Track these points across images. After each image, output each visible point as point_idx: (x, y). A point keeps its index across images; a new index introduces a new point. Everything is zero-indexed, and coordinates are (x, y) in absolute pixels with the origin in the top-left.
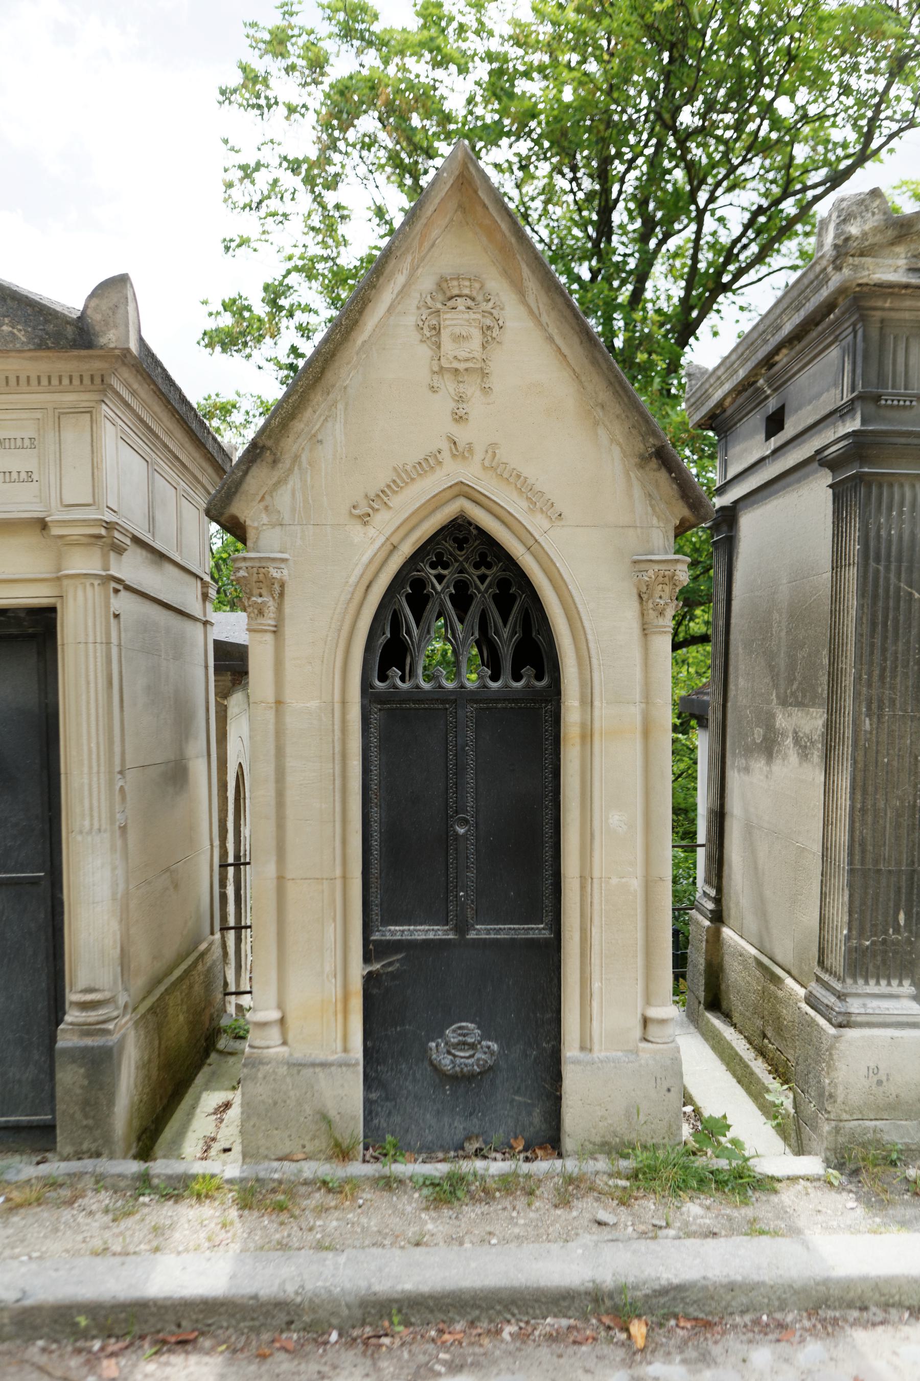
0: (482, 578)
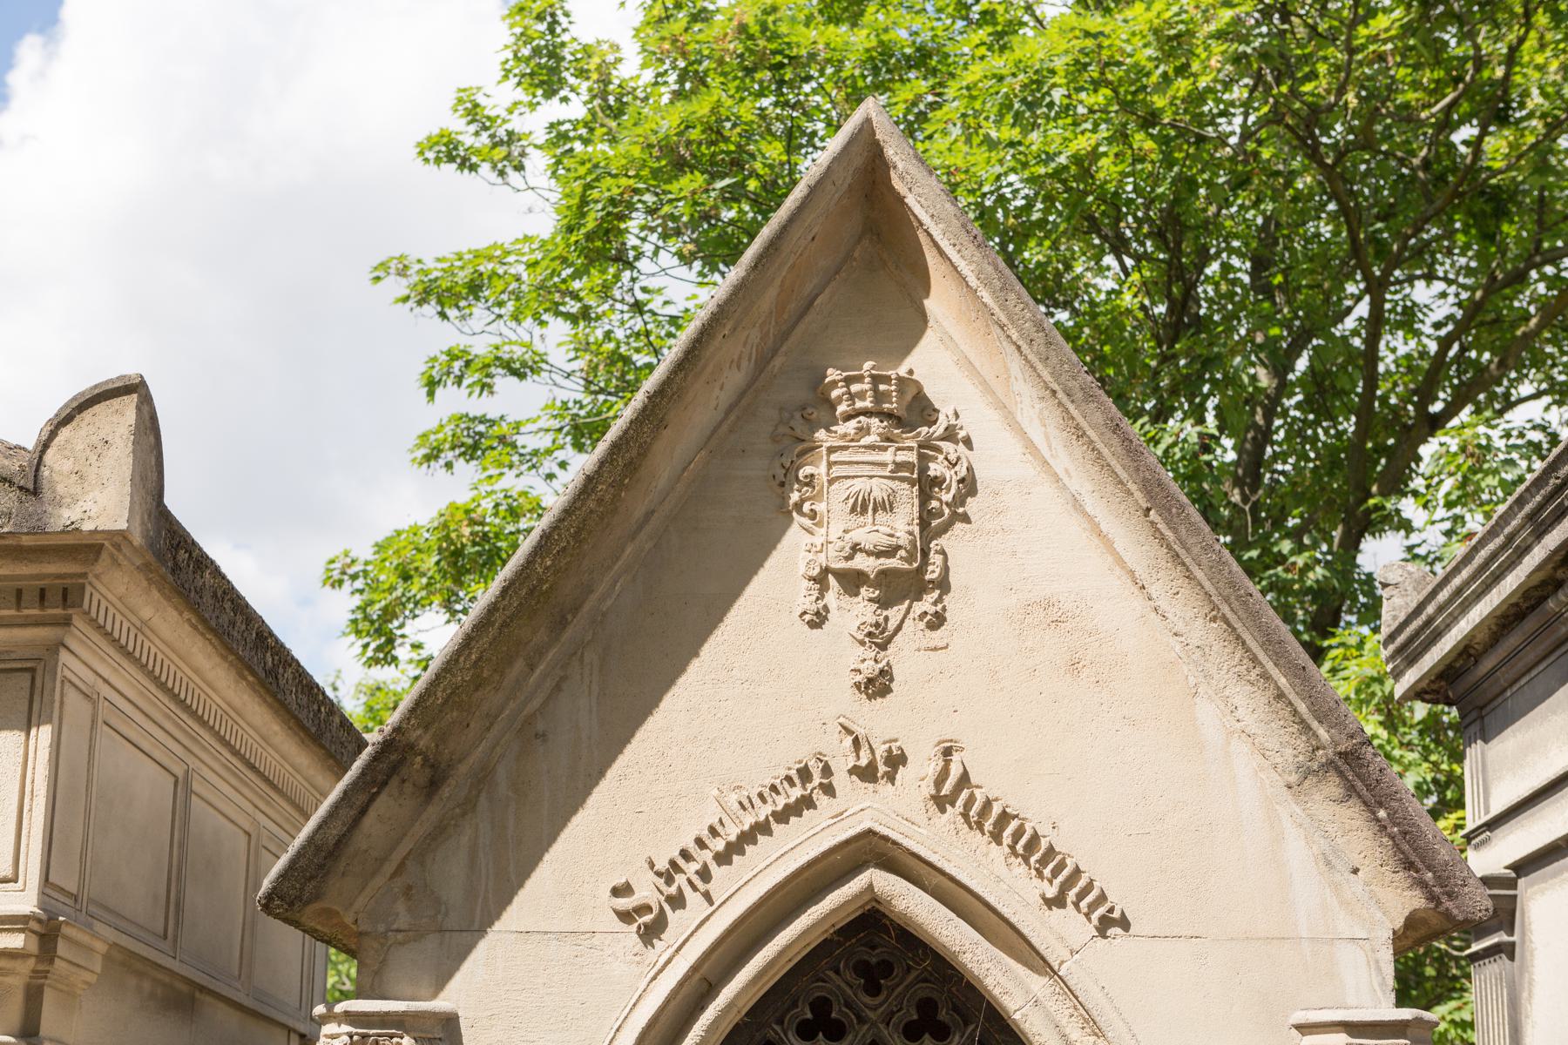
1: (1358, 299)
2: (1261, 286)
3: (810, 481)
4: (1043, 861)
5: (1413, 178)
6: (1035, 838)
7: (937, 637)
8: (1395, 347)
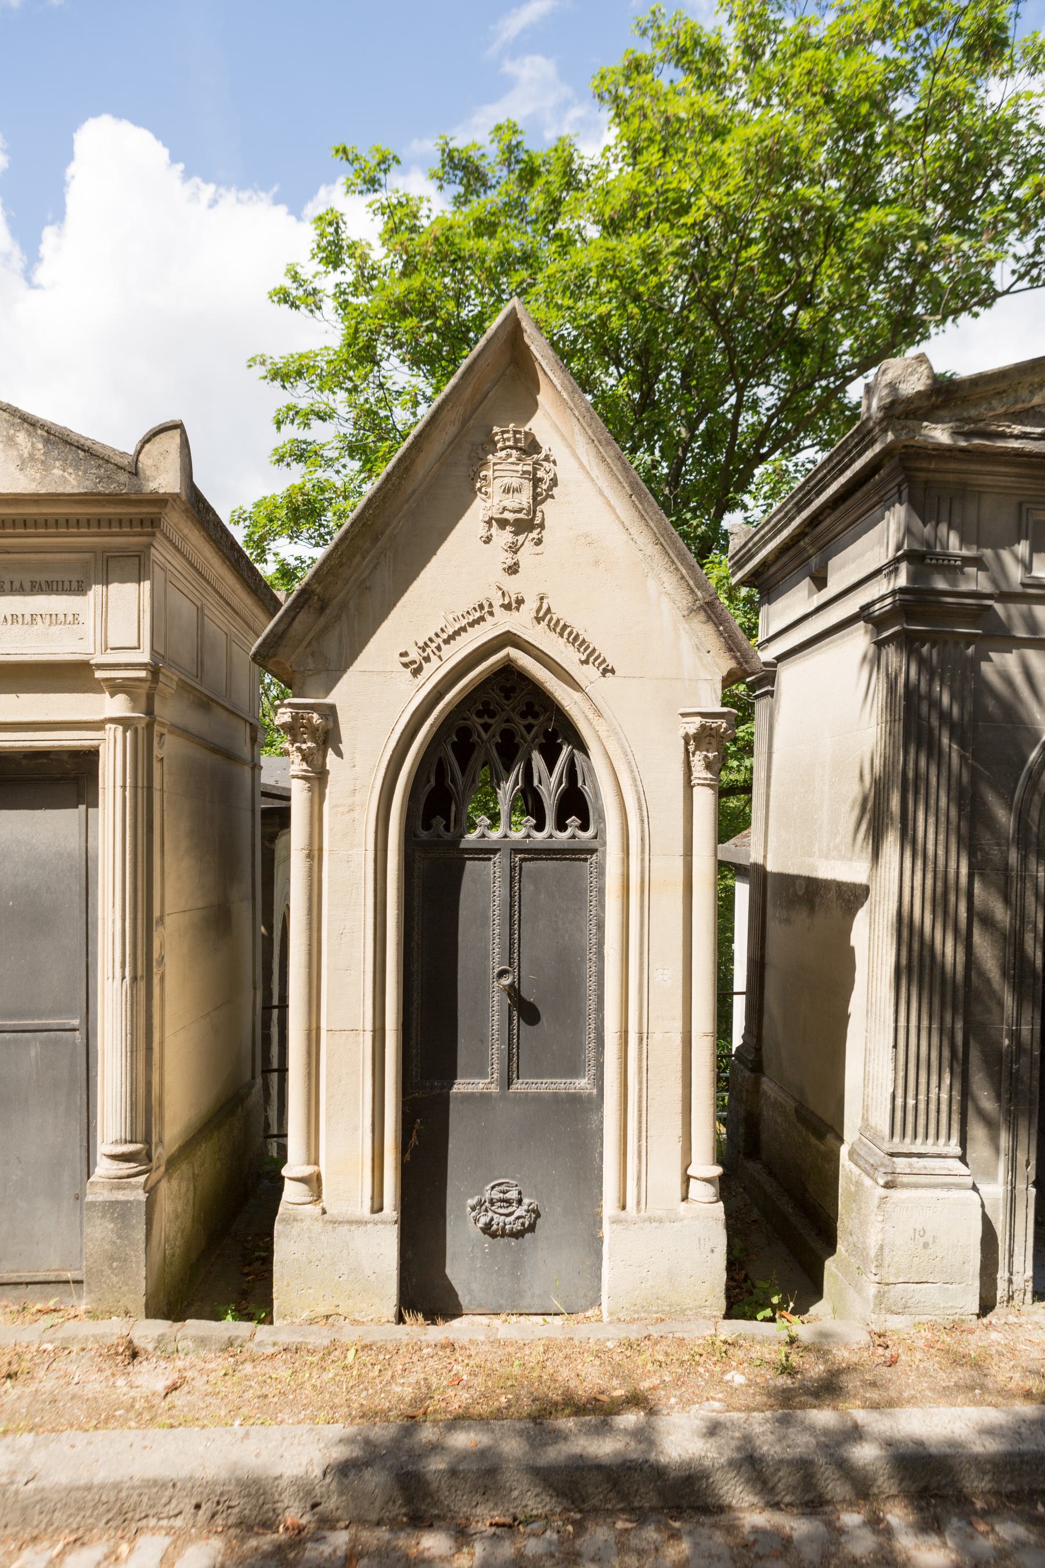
0: (529, 728)
1: (731, 394)
2: (685, 386)
3: (485, 478)
4: (580, 645)
5: (762, 332)
6: (577, 635)
7: (539, 549)
8: (747, 419)
